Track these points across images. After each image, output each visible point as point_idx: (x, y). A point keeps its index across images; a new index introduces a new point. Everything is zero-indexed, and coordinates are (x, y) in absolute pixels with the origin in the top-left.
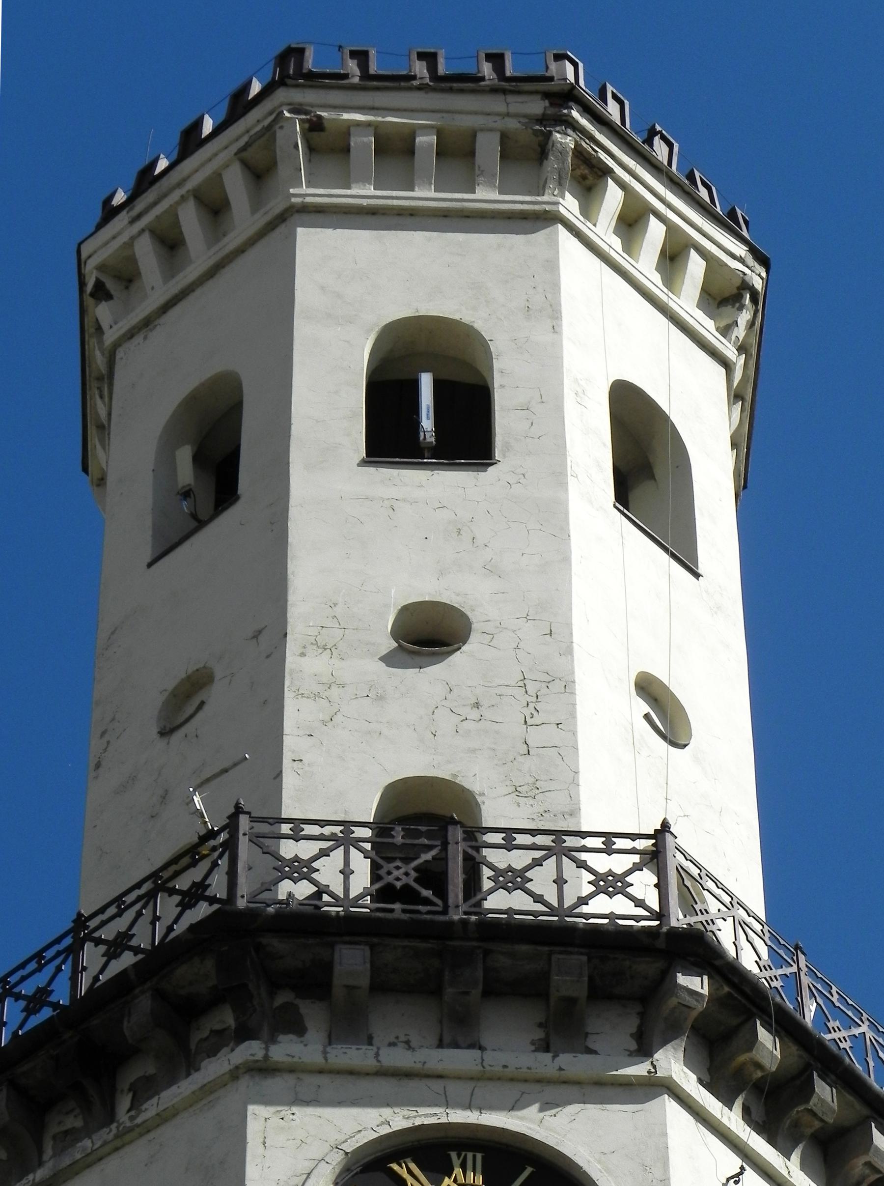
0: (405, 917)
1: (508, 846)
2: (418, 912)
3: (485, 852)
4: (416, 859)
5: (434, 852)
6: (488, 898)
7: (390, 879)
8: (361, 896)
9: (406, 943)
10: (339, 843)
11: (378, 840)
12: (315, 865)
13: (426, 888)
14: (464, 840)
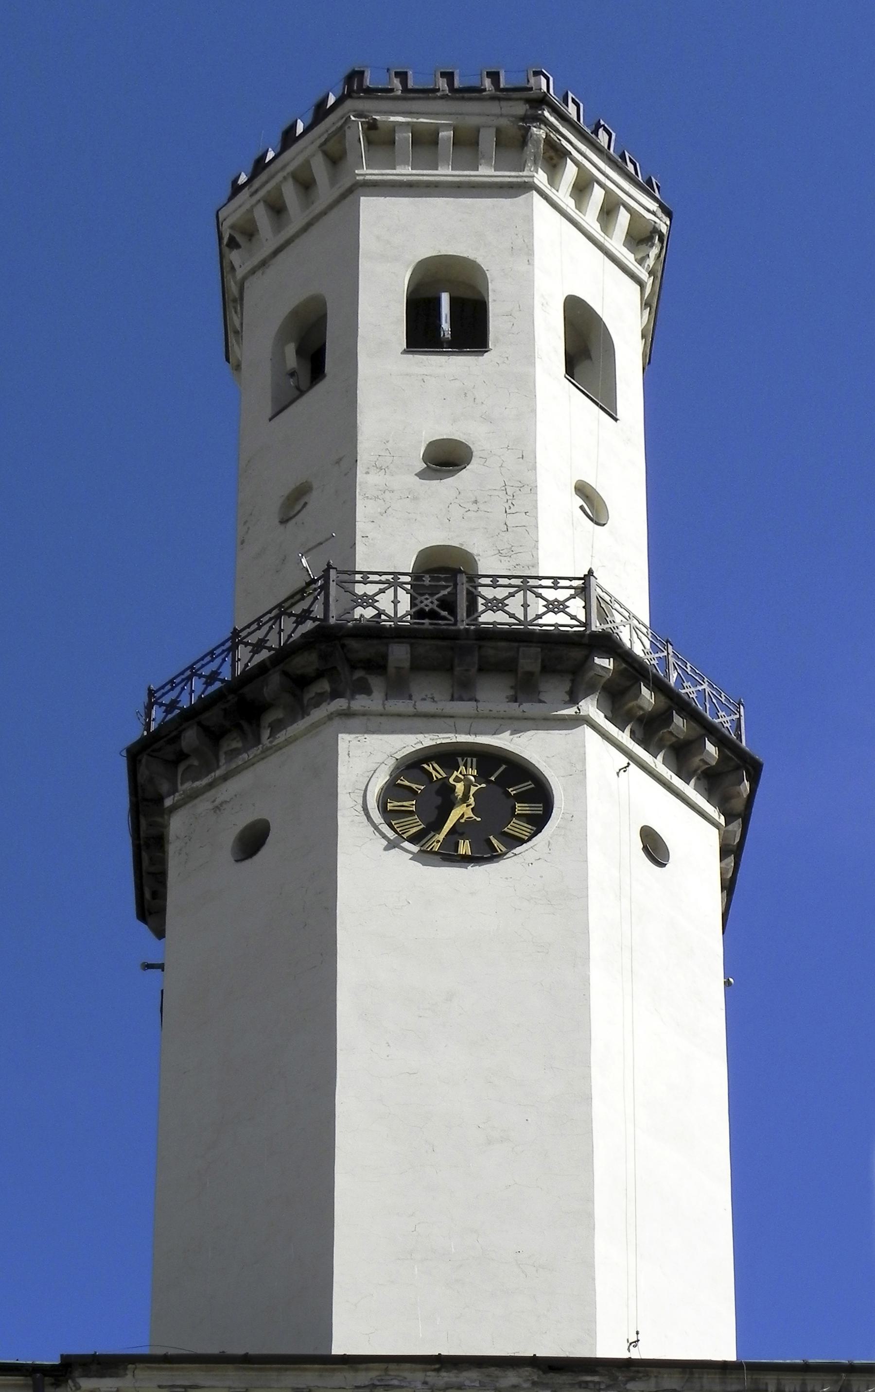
0: (431, 627)
2: (439, 624)
5: (449, 590)
7: (422, 605)
9: (432, 642)
12: (567, 604)
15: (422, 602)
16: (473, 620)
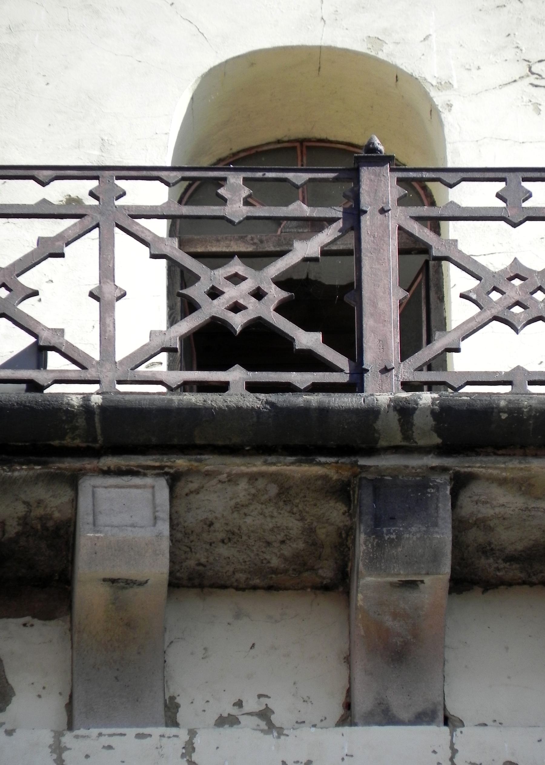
0: (255, 401)
1: (510, 214)
2: (288, 388)
3: (454, 230)
4: (280, 254)
5: (326, 237)
6: (463, 345)
7: (217, 308)
8: (145, 355)
9: (258, 465)
10: (88, 222)
11: (186, 210)
12: (28, 280)
13: (308, 327)
14: (402, 201)
15: (214, 293)
16: (429, 366)
